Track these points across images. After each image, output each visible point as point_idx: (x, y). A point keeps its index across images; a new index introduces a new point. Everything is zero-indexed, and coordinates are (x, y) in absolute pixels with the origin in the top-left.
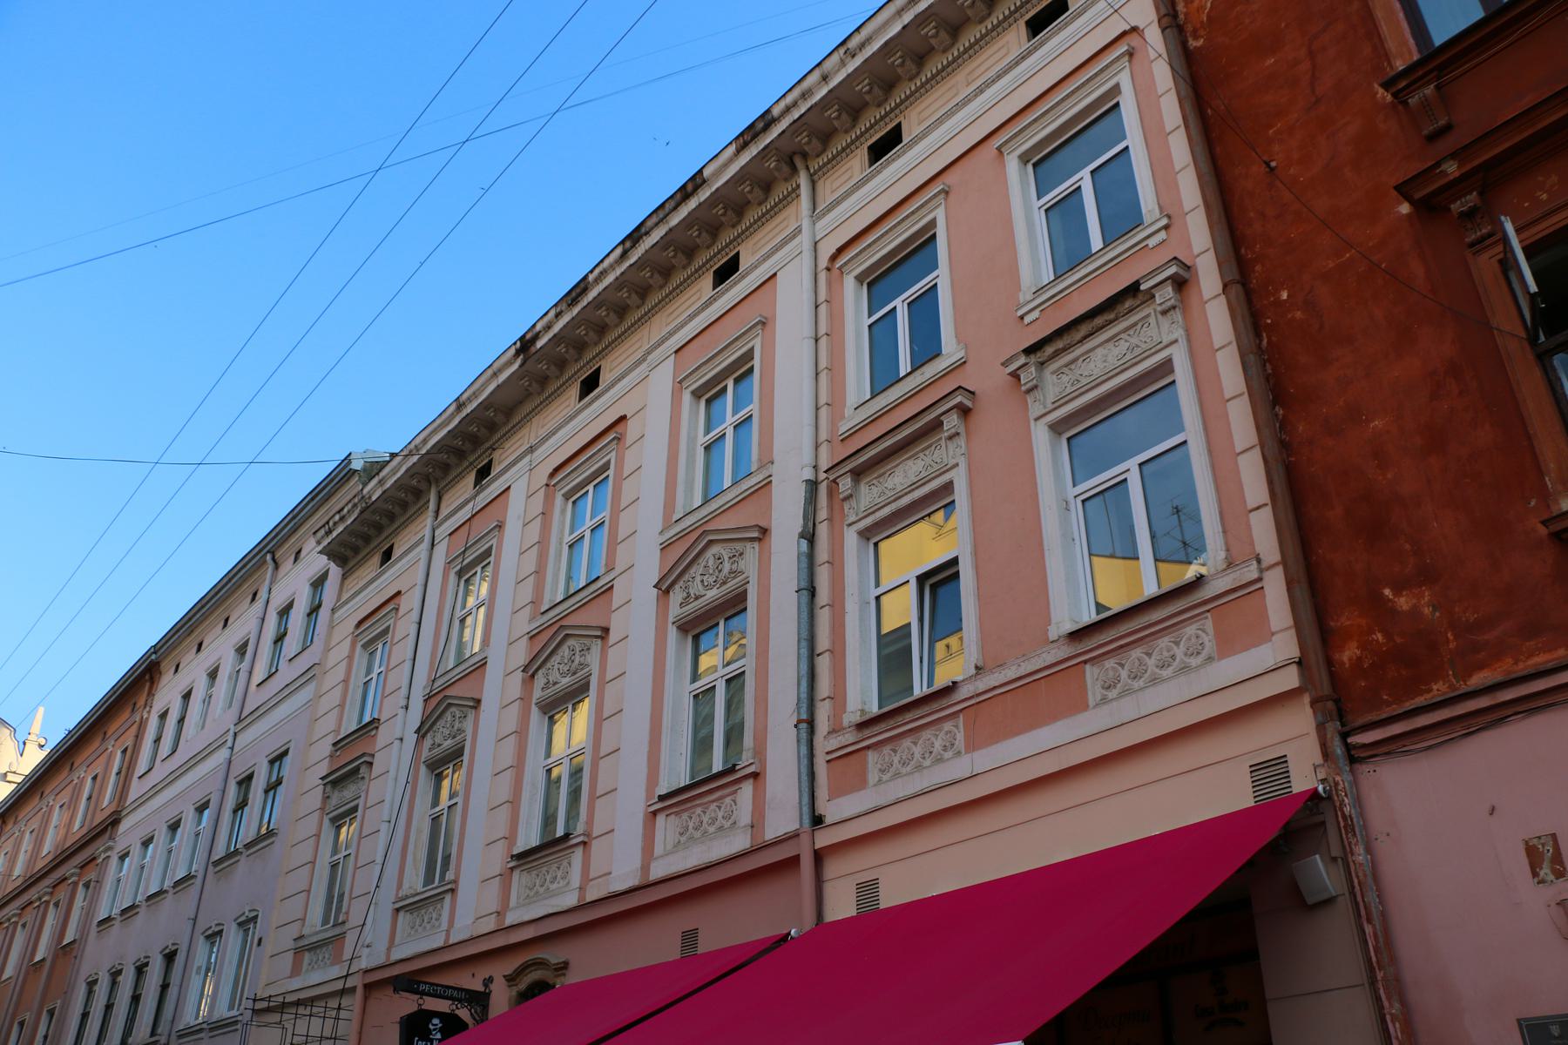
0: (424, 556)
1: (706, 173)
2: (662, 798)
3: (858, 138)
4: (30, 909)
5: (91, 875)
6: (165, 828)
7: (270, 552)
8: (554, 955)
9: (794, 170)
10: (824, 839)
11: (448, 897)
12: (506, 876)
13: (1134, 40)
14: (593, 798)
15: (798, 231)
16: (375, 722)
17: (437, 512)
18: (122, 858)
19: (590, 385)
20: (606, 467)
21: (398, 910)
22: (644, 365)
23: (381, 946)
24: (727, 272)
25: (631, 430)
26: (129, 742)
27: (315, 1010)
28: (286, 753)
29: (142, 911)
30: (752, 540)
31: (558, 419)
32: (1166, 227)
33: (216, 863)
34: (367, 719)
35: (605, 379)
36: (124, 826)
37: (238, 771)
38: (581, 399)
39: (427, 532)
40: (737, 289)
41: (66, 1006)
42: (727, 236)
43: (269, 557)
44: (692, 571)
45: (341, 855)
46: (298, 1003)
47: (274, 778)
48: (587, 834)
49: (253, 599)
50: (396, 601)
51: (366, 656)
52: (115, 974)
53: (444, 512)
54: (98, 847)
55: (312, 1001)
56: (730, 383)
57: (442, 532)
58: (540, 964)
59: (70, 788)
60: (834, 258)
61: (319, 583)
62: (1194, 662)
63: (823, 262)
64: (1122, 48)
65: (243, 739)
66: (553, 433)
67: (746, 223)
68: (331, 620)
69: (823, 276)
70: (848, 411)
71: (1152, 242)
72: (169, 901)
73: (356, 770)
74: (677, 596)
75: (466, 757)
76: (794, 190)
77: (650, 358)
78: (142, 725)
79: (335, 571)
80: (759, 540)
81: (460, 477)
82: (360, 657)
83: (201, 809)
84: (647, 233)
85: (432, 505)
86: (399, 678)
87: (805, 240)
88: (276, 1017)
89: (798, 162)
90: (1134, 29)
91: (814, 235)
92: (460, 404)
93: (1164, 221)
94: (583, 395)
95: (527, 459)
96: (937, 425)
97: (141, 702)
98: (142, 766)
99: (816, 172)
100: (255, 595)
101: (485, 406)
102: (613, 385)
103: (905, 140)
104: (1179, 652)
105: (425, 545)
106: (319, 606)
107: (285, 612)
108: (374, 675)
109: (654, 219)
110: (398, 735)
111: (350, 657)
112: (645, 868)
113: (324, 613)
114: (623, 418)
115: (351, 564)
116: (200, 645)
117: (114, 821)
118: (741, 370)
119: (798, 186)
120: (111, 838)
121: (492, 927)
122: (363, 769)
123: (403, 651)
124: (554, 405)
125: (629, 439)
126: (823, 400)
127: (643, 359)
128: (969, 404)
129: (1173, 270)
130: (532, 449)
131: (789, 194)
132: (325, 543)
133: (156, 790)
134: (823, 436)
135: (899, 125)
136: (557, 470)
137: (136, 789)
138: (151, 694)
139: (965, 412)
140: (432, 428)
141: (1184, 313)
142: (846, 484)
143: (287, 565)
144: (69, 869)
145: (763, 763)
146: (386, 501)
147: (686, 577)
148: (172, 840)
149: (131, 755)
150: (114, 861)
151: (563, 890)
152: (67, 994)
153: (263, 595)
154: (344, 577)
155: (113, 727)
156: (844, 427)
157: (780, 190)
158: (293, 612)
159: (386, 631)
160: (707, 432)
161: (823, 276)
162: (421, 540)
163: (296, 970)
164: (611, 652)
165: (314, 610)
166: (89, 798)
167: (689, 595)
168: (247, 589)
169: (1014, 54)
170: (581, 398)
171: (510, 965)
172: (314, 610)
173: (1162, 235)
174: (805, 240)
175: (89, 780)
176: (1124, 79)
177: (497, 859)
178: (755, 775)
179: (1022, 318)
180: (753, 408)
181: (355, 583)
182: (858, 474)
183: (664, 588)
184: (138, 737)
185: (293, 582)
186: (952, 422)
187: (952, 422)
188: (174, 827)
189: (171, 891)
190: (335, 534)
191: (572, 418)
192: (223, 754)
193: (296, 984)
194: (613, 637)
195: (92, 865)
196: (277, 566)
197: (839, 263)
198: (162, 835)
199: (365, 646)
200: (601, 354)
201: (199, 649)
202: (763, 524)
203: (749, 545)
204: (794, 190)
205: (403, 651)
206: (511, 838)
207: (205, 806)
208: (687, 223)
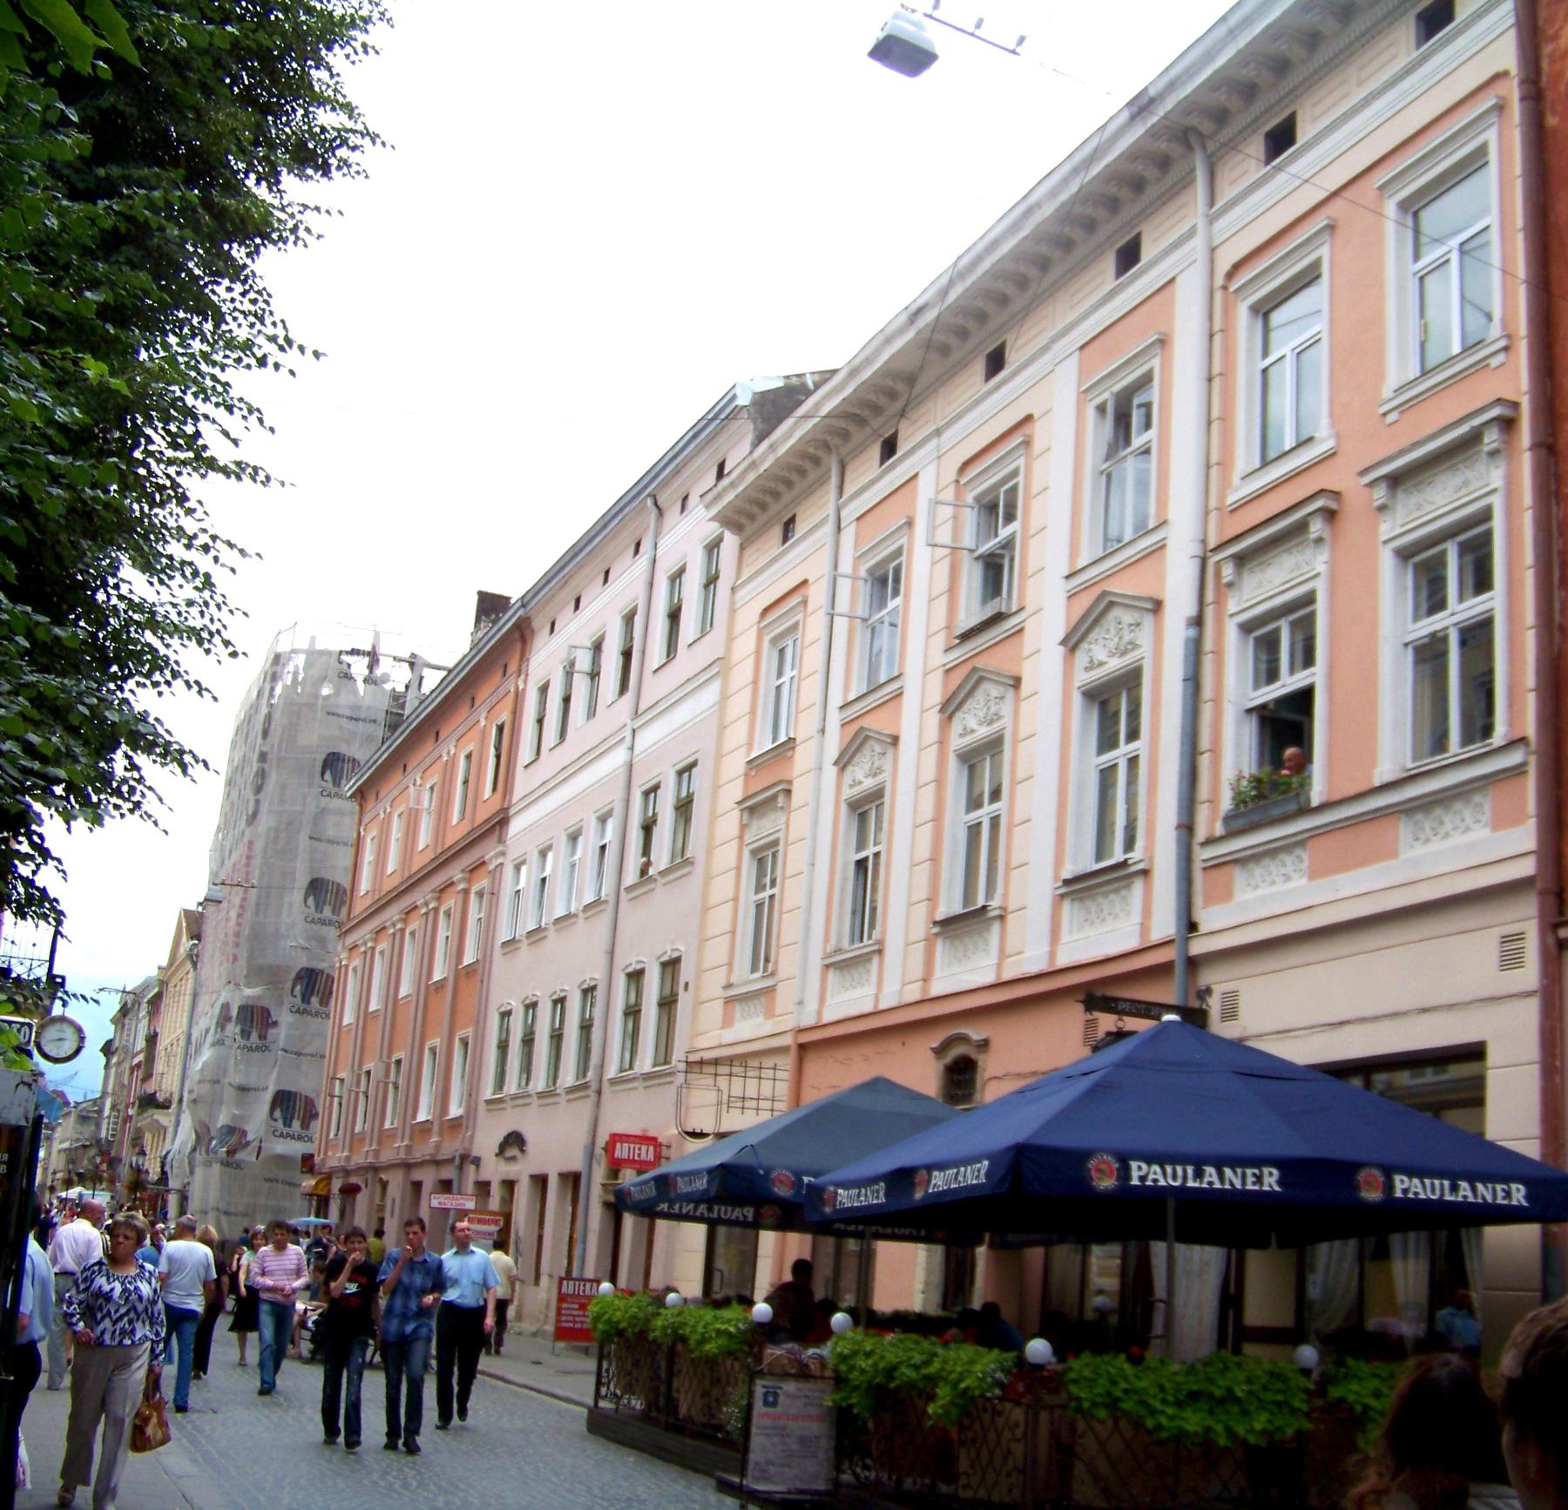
0: (829, 541)
2: (1067, 882)
4: (414, 915)
5: (482, 883)
6: (564, 838)
7: (650, 497)
8: (975, 1033)
9: (1190, 147)
10: (1198, 947)
11: (876, 959)
12: (930, 941)
14: (1008, 868)
15: (1192, 233)
17: (1212, 201)
18: (518, 868)
19: (1281, 140)
20: (1015, 474)
21: (828, 966)
23: (811, 1006)
25: (1038, 430)
26: (504, 716)
27: (735, 1070)
28: (694, 764)
29: (551, 933)
31: (1385, 75)
32: (1506, 349)
33: (630, 889)
34: (783, 738)
35: (1304, 134)
36: (515, 827)
37: (641, 782)
38: (882, 463)
39: (830, 510)
40: (1142, 283)
41: (480, 1036)
42: (1127, 213)
43: (649, 502)
47: (684, 794)
48: (1004, 908)
49: (637, 552)
50: (802, 591)
51: (776, 655)
52: (532, 1006)
53: (850, 489)
54: (489, 850)
57: (851, 512)
58: (963, 1039)
59: (438, 767)
60: (1230, 275)
61: (713, 547)
63: (1219, 280)
65: (646, 739)
66: (959, 416)
68: (732, 603)
69: (1218, 295)
70: (1236, 480)
71: (1494, 362)
72: (580, 925)
73: (774, 798)
75: (887, 799)
78: (519, 698)
79: (731, 541)
83: (603, 820)
85: (834, 481)
86: (811, 690)
87: (1198, 244)
88: (711, 1069)
89: (1193, 140)
91: (1210, 238)
92: (1141, 106)
93: (1502, 343)
94: (785, 539)
95: (933, 443)
96: (1301, 527)
97: (513, 667)
98: (525, 753)
99: (1213, 154)
100: (638, 545)
101: (1188, 106)
105: (829, 528)
106: (716, 577)
107: (677, 577)
108: (785, 679)
111: (758, 652)
112: (1052, 955)
113: (723, 585)
114: (1028, 419)
116: (578, 601)
117: (499, 823)
119: (1193, 170)
120: (501, 841)
121: (916, 996)
122: (781, 800)
123: (813, 658)
125: (1037, 446)
126: (1214, 458)
127: (1046, 349)
128: (1333, 505)
129: (1495, 412)
130: (938, 432)
133: (547, 788)
134: (1213, 503)
136: (766, 611)
137: (523, 782)
138: (524, 658)
139: (1330, 515)
140: (1205, 48)
141: (1333, 550)
142: (1228, 571)
143: (672, 514)
144: (455, 872)
145: (1151, 859)
146: (1085, 201)
148: (573, 853)
149: (506, 738)
150: (509, 870)
151: (968, 971)
152: (480, 1022)
153: (646, 547)
154: (742, 548)
155: (484, 693)
156: (1232, 498)
157: (1175, 174)
158: (686, 578)
159: (795, 627)
161: (1218, 295)
162: (825, 520)
163: (727, 1022)
164: (1024, 705)
165: (711, 581)
166: (466, 782)
168: (627, 538)
169: (1402, 62)
170: (882, 463)
171: (937, 1038)
172: (711, 581)
173: (1501, 358)
174: (1198, 244)
175: (462, 762)
177: (920, 928)
178: (1145, 873)
179: (1384, 414)
181: (756, 558)
182: (1241, 560)
184: (516, 713)
185: (686, 535)
186: (1317, 527)
187: (1317, 527)
188: (574, 838)
189: (525, 942)
191: (978, 402)
192: (619, 757)
193: (729, 1036)
194: (1026, 688)
195: (482, 871)
196: (660, 512)
198: (562, 843)
199: (774, 641)
201: (577, 607)
202: (1156, 595)
205: (813, 658)
206: (932, 900)
207: (609, 814)
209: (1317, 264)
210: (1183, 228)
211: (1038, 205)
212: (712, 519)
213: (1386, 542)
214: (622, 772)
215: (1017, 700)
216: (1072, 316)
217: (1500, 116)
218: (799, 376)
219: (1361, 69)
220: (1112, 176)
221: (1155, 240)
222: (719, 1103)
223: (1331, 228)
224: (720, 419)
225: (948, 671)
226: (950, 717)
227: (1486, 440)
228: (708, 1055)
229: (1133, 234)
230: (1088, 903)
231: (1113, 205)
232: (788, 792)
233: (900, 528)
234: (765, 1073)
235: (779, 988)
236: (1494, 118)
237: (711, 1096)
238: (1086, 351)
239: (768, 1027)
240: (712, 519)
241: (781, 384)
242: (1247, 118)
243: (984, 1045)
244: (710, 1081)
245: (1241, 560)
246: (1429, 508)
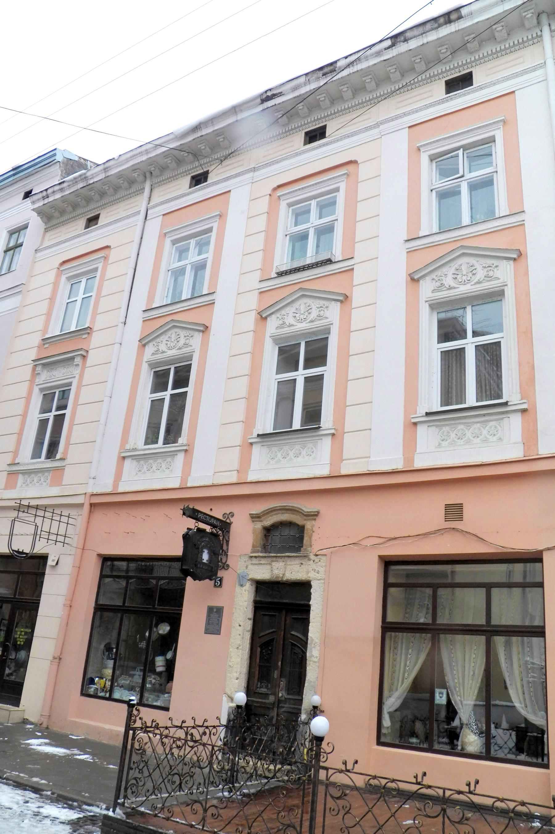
1: (339, 64)
3: (160, 182)
8: (308, 506)
13: (351, 168)
16: (88, 330)
19: (93, 221)
22: (376, 131)
24: (199, 180)
30: (199, 331)
44: (161, 338)
45: (54, 413)
46: (37, 507)
55: (45, 508)
56: (84, 281)
62: (491, 439)
64: (343, 171)
67: (132, 190)
71: (84, 336)
73: (73, 358)
74: (150, 350)
76: (142, 189)
77: (382, 127)
80: (203, 332)
81: (74, 219)
82: (64, 286)
84: (406, 40)
88: (33, 511)
90: (355, 162)
94: (87, 227)
95: (251, 174)
102: (338, 140)
103: (209, 181)
104: (485, 432)
109: (416, 32)
110: (118, 340)
114: (108, 247)
115: (54, 222)
118: (202, 237)
119: (144, 188)
124: (170, 185)
128: (84, 354)
131: (139, 190)
132: (41, 204)
135: (99, 214)
147: (158, 340)
160: (69, 299)
162: (138, 213)
167: (158, 350)
176: (343, 186)
180: (209, 255)
183: (143, 343)
186: (78, 360)
190: (51, 199)
191: (297, 154)
197: (280, 193)
199: (69, 279)
200: (478, 62)
203: (196, 334)
204: (142, 189)
208: (440, 42)
209: (212, 227)
210: (136, 210)
211: (161, 146)
212: (33, 210)
213: (37, 385)
214: (71, 296)
215: (84, 367)
216: (124, 214)
217: (347, 178)
218: (85, 160)
219: (107, 213)
220: (151, 162)
221: (106, 217)
222: (35, 535)
223: (347, 175)
224: (45, 162)
225: (261, 293)
226: (144, 346)
227: (76, 360)
228: (33, 503)
229: (98, 213)
230: (275, 449)
231: (88, 200)
232: (84, 357)
233: (216, 216)
234: (64, 519)
235: (66, 468)
236: (217, 219)
237: (31, 529)
238: (165, 217)
239: (55, 491)
240: (33, 210)
241: (76, 159)
242: (189, 167)
243: (315, 515)
244: (32, 519)
245: (44, 365)
246: (53, 377)
